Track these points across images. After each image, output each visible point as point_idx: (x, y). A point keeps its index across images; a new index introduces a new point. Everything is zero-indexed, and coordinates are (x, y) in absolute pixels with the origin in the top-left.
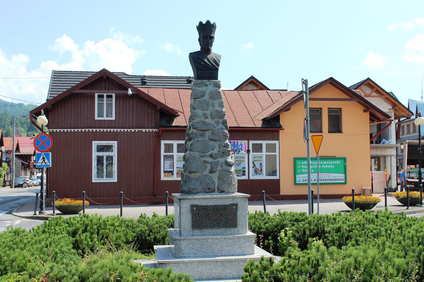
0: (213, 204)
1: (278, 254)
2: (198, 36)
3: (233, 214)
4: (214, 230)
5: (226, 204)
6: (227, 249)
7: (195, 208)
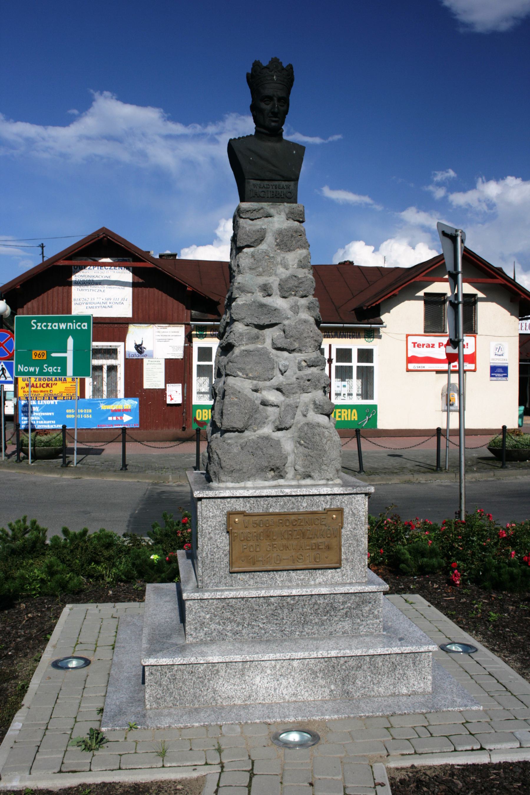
1: (522, 765)
2: (251, 99)
6: (317, 620)
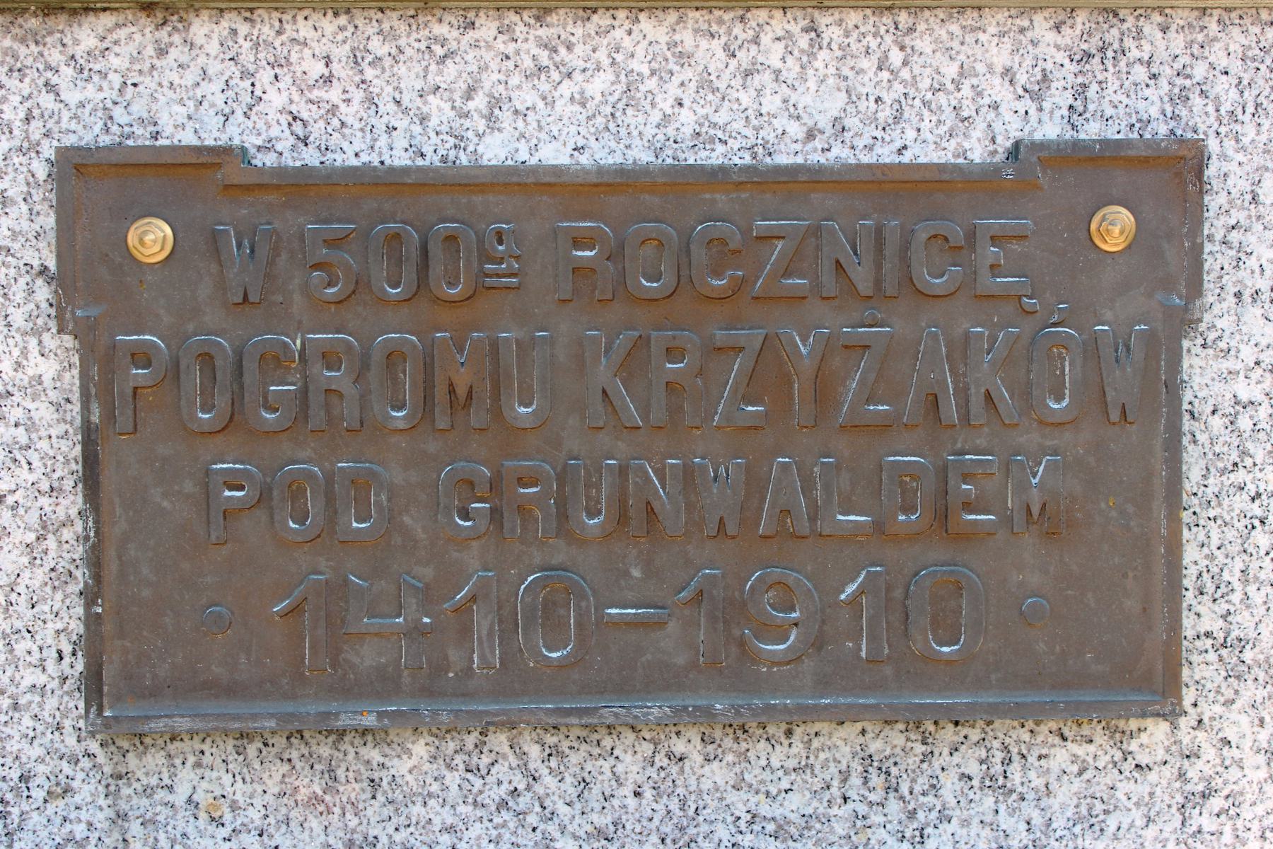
0: (604, 154)
3: (1096, 397)
4: (631, 760)
5: (925, 144)
7: (153, 238)
